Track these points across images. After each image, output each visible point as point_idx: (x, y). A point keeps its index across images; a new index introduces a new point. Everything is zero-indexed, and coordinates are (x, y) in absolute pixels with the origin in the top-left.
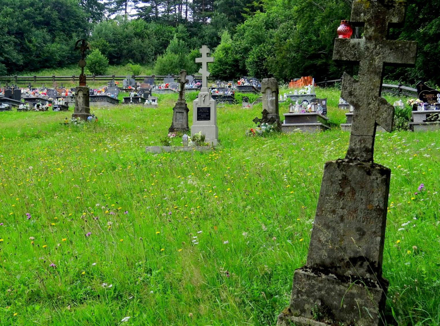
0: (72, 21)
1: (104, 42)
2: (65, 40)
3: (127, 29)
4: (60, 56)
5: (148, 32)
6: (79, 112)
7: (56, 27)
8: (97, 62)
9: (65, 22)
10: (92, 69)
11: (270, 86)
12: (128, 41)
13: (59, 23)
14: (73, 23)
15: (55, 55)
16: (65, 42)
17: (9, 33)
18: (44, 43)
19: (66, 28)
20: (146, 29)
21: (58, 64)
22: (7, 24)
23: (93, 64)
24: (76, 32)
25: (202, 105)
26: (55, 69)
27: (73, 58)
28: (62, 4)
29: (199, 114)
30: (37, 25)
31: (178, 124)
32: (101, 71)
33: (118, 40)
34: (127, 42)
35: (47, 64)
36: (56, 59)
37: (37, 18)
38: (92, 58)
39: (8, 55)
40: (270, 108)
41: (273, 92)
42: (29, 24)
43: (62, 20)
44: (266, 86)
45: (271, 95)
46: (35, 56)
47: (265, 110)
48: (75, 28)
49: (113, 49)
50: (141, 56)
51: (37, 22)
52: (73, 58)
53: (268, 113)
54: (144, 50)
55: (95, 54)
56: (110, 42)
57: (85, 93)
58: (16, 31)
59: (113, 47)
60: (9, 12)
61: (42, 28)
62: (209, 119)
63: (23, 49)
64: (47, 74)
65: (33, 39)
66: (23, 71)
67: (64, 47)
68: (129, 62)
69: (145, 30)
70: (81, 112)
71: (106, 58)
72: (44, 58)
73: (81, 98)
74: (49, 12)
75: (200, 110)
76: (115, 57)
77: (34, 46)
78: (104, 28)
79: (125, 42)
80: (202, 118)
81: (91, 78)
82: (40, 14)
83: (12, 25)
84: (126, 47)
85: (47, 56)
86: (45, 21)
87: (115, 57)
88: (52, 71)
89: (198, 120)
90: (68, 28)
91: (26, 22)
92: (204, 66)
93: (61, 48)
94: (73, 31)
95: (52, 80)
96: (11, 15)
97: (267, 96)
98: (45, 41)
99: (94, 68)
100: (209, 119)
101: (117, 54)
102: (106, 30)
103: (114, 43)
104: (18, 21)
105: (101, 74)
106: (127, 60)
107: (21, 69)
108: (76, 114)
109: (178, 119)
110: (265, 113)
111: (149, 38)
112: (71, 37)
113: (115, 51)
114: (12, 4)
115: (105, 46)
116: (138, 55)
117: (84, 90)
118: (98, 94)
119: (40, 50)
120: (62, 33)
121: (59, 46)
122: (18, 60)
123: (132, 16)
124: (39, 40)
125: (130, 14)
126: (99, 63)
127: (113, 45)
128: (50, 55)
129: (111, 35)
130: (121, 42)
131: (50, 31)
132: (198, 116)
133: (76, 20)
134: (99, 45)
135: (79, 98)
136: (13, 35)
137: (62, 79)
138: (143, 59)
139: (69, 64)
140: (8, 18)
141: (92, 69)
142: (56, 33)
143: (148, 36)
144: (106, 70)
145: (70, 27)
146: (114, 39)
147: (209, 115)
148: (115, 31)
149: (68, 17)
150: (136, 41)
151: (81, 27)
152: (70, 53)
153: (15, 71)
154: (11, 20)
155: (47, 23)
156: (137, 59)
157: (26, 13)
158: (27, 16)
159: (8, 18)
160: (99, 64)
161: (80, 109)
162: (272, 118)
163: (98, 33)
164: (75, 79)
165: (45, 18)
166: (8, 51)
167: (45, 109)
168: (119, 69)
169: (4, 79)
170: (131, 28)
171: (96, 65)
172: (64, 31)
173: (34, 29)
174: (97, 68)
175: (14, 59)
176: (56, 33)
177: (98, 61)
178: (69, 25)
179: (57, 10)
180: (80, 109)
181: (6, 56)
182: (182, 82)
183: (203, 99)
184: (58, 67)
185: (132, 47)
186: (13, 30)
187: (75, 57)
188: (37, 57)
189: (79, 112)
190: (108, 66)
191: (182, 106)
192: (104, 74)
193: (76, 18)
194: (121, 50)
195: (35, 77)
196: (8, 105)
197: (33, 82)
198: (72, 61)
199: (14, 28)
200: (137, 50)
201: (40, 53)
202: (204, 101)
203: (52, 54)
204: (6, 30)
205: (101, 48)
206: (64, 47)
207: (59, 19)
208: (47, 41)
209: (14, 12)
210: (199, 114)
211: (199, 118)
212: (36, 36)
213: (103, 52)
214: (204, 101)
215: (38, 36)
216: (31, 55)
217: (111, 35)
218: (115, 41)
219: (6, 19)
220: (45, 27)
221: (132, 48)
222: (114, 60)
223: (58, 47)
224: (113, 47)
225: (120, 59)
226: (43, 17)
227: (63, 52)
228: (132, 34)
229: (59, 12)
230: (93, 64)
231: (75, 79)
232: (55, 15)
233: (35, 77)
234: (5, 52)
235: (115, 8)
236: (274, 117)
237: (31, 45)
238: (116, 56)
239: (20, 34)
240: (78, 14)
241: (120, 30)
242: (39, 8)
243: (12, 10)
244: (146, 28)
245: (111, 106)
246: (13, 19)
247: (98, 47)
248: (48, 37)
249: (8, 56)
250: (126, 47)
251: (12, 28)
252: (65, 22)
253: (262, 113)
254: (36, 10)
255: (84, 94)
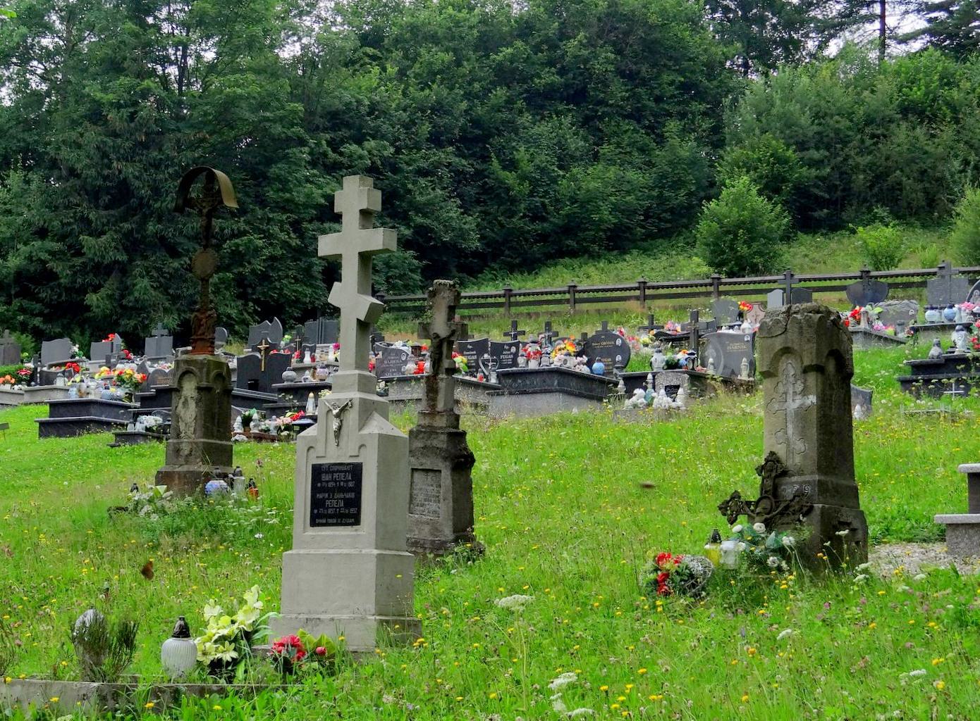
0: (666, 78)
1: (778, 145)
2: (642, 150)
3: (873, 92)
4: (615, 209)
5: (955, 94)
6: (182, 460)
7: (607, 105)
8: (741, 224)
9: (644, 82)
10: (723, 252)
11: (793, 338)
12: (873, 136)
13: (618, 90)
14: (672, 83)
15: (598, 207)
16: (638, 158)
17: (436, 140)
18: (560, 167)
19: (644, 106)
20: (948, 84)
21: (609, 239)
22: (432, 109)
23: (728, 232)
24: (682, 116)
25: (334, 455)
26: (595, 257)
27: (667, 216)
28: (630, 18)
29: (320, 496)
30: (540, 101)
31: (418, 522)
32: (757, 260)
33: (832, 135)
34: (868, 142)
35: (569, 242)
36: (601, 220)
37: (540, 78)
38: (725, 210)
39: (425, 215)
40: (799, 451)
41: (806, 371)
42: (510, 101)
43: (630, 77)
44: (778, 344)
45: (799, 387)
46: (525, 216)
47: (773, 459)
48: (679, 103)
49: (814, 172)
50: (925, 191)
51: (538, 94)
52: (667, 216)
53: (785, 473)
54: (934, 168)
55: (739, 196)
56: (802, 146)
57: (204, 384)
58: (462, 129)
59: (813, 164)
60: (436, 68)
61: (558, 113)
62: (355, 520)
63: (482, 193)
64: (556, 279)
65: (522, 154)
66: (481, 272)
67: (631, 175)
68: (875, 218)
69: (944, 92)
70: (187, 462)
71: (779, 208)
72: (561, 223)
73: (192, 405)
74: (585, 52)
75: (325, 477)
76: (821, 203)
77: (523, 178)
78: (777, 98)
79: (863, 141)
80: (331, 516)
81: (703, 289)
82: (551, 63)
83: (447, 113)
84: (864, 160)
85: (567, 216)
86: (567, 86)
87: (821, 203)
88: (585, 268)
89: (314, 523)
90: (652, 104)
91: (500, 93)
92: (350, 270)
93: (620, 181)
94: (670, 115)
95: (568, 301)
96: (444, 75)
97: (781, 389)
98: (565, 160)
99: (732, 249)
100: (355, 520)
101: (832, 189)
102: (786, 99)
103: (817, 149)
104: (468, 96)
105: (755, 270)
106: (870, 210)
107: (472, 265)
108: (169, 469)
109: (420, 498)
110: (773, 470)
111: (957, 121)
112: (661, 140)
113: (823, 179)
114: (453, 38)
115: (782, 161)
116: (913, 189)
117: (201, 370)
118: (533, 365)
119: (546, 192)
120: (627, 125)
121: (612, 172)
122: (463, 234)
123: (905, 40)
124: (542, 158)
125: (900, 32)
126: (750, 229)
127: (815, 154)
128: (582, 206)
129: (805, 120)
130: (845, 142)
131: (586, 122)
132: (316, 504)
133: (681, 72)
134: (760, 160)
135: (185, 403)
136: (451, 144)
137: (608, 294)
138: (931, 202)
139: (650, 236)
140: (435, 86)
141: (723, 252)
142: (606, 127)
143: (955, 110)
144: (776, 255)
145: (658, 100)
146: (818, 133)
147: (356, 503)
148: (823, 103)
149: (653, 66)
150: (902, 135)
151: (701, 96)
152: (652, 198)
153: (454, 270)
154: (445, 92)
155: (577, 94)
156: (909, 206)
157: (500, 64)
158: (504, 75)
159: (435, 86)
160: (749, 231)
161: (186, 449)
162: (799, 494)
163: (759, 115)
164: (648, 292)
165: (571, 75)
166: (429, 203)
167: (274, 433)
168: (833, 245)
169: (409, 304)
170: (885, 86)
171: (736, 235)
172: (636, 115)
173: (527, 118)
174: (743, 250)
175: (448, 228)
176: (606, 127)
177: (743, 222)
178: (657, 92)
179: (614, 44)
180: (186, 449)
181: (420, 220)
182: (437, 336)
183: (335, 425)
184: (609, 249)
185: (887, 159)
186: (448, 129)
187: (672, 211)
188: (534, 219)
189: (182, 460)
190: (787, 238)
191: (435, 443)
192: (767, 271)
193: (685, 64)
194: (844, 174)
195: (509, 293)
196: (160, 419)
197: (502, 310)
198: (663, 225)
199: (457, 123)
200: (907, 170)
201: (543, 204)
202: (338, 433)
203: (586, 203)
204: (426, 128)
205: (764, 169)
206: (631, 175)
207: (621, 73)
208: (572, 157)
209: (458, 63)
210: (320, 496)
211: (320, 517)
212: (533, 142)
213: (771, 187)
214: (338, 433)
215: (541, 137)
216: (512, 214)
217: (805, 120)
218: (821, 141)
219: (427, 91)
220: (569, 110)
221: (890, 163)
222: (816, 214)
223: (605, 180)
224: (813, 164)
225: (843, 208)
226: (562, 72)
227: (628, 193)
228: (891, 112)
229: (619, 52)
230: (728, 232)
231: (648, 292)
232: (604, 59)
233: (509, 293)
234: (419, 210)
235: (841, 15)
236: (808, 489)
237: (510, 178)
238: (827, 196)
239: (476, 139)
240: (693, 51)
241: (844, 99)
242: (547, 40)
243: (448, 57)
244: (948, 81)
245: (579, 409)
246: (451, 88)
247: (756, 169)
248: (576, 144)
249: (428, 221)
250: (864, 160)
251: (447, 120)
252: (644, 82)
253: (760, 470)
254: (537, 49)
255: (199, 389)
